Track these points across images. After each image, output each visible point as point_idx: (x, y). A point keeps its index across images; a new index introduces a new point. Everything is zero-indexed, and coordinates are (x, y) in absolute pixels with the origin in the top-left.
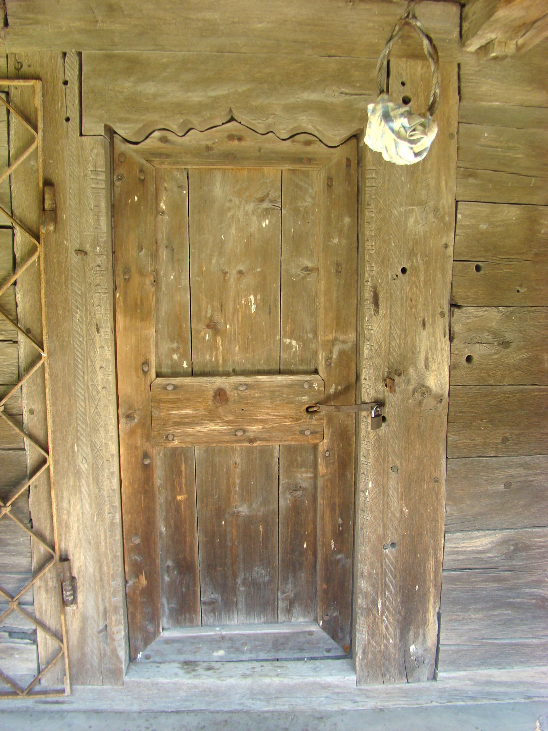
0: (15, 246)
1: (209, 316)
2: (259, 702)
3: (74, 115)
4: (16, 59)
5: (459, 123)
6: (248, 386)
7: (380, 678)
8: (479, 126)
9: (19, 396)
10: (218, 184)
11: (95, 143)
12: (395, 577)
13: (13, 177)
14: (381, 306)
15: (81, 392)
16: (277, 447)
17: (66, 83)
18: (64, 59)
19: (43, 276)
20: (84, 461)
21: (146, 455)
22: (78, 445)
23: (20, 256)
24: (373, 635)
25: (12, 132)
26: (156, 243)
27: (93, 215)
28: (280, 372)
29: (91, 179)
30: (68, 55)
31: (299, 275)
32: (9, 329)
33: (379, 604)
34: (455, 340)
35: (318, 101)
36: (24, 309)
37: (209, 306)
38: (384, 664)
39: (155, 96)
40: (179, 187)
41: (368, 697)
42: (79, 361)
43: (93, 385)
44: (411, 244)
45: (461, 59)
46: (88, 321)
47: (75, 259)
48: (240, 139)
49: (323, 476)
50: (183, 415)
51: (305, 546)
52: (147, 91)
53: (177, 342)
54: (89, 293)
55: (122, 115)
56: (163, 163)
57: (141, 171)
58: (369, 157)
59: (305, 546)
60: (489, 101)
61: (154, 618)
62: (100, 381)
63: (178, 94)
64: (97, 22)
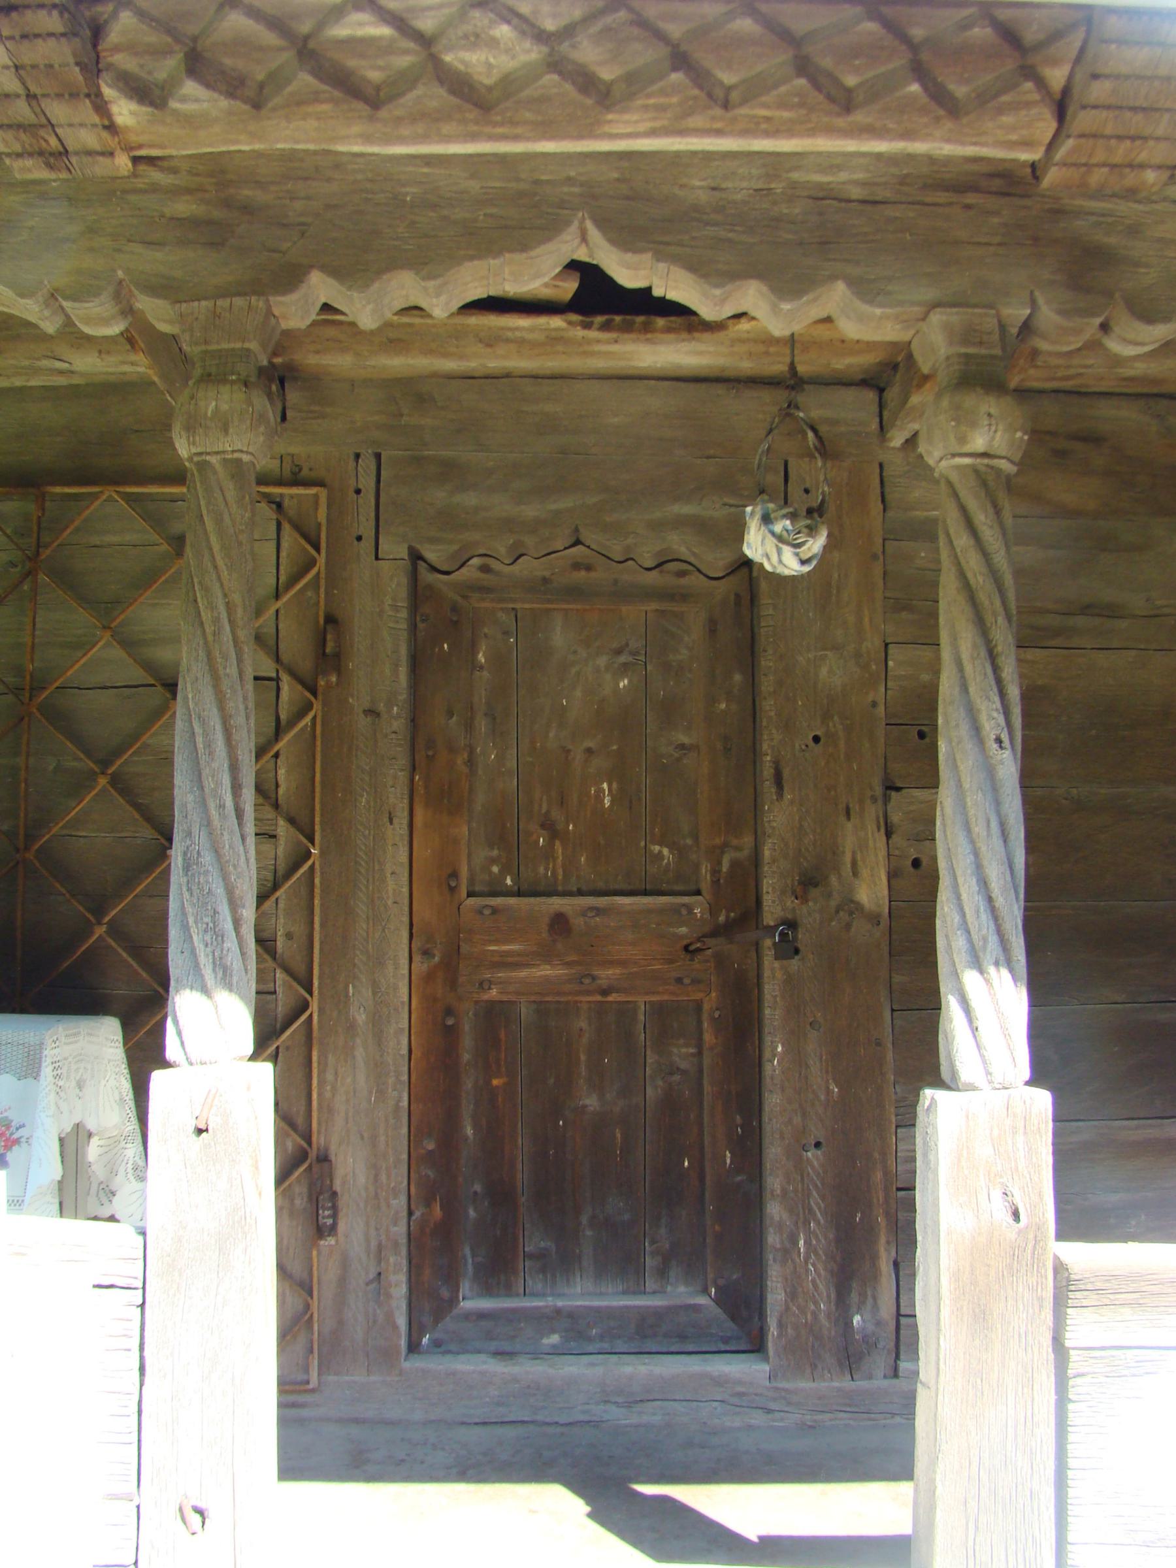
0: (280, 704)
1: (544, 810)
2: (613, 1408)
3: (368, 531)
4: (293, 462)
5: (884, 540)
6: (598, 911)
7: (808, 1371)
10: (558, 629)
12: (823, 1198)
14: (786, 789)
15: (362, 909)
16: (643, 1007)
17: (358, 492)
18: (357, 462)
19: (319, 743)
20: (362, 1009)
21: (449, 1012)
22: (354, 987)
24: (792, 1295)
25: (283, 554)
26: (472, 708)
28: (645, 893)
30: (362, 456)
31: (672, 755)
33: (801, 1243)
34: (894, 836)
37: (545, 797)
38: (813, 1346)
41: (789, 1404)
44: (825, 701)
47: (363, 722)
48: (589, 568)
49: (711, 1049)
50: (504, 952)
51: (686, 1164)
53: (499, 849)
58: (764, 586)
59: (686, 1164)
61: (451, 1277)
64: (402, 415)
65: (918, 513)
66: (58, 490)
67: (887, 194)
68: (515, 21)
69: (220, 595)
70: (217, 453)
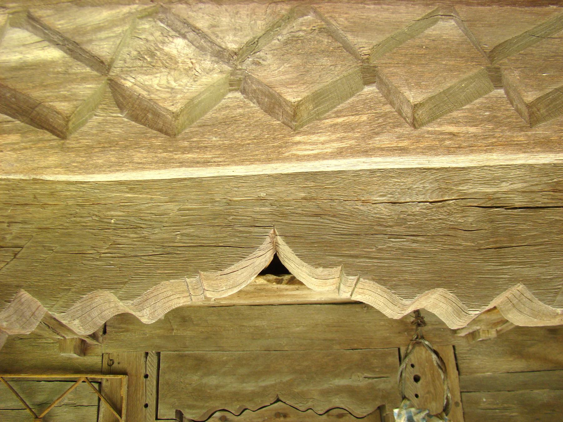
3: (152, 402)
4: (109, 357)
5: (461, 392)
8: (478, 394)
17: (146, 376)
18: (146, 358)
25: (101, 415)
30: (149, 355)
35: (347, 385)
39: (217, 387)
45: (455, 342)
52: (211, 383)
55: (190, 403)
60: (481, 373)
63: (235, 385)
64: (173, 330)
65: (479, 374)
67: (541, 201)
68: (191, 35)
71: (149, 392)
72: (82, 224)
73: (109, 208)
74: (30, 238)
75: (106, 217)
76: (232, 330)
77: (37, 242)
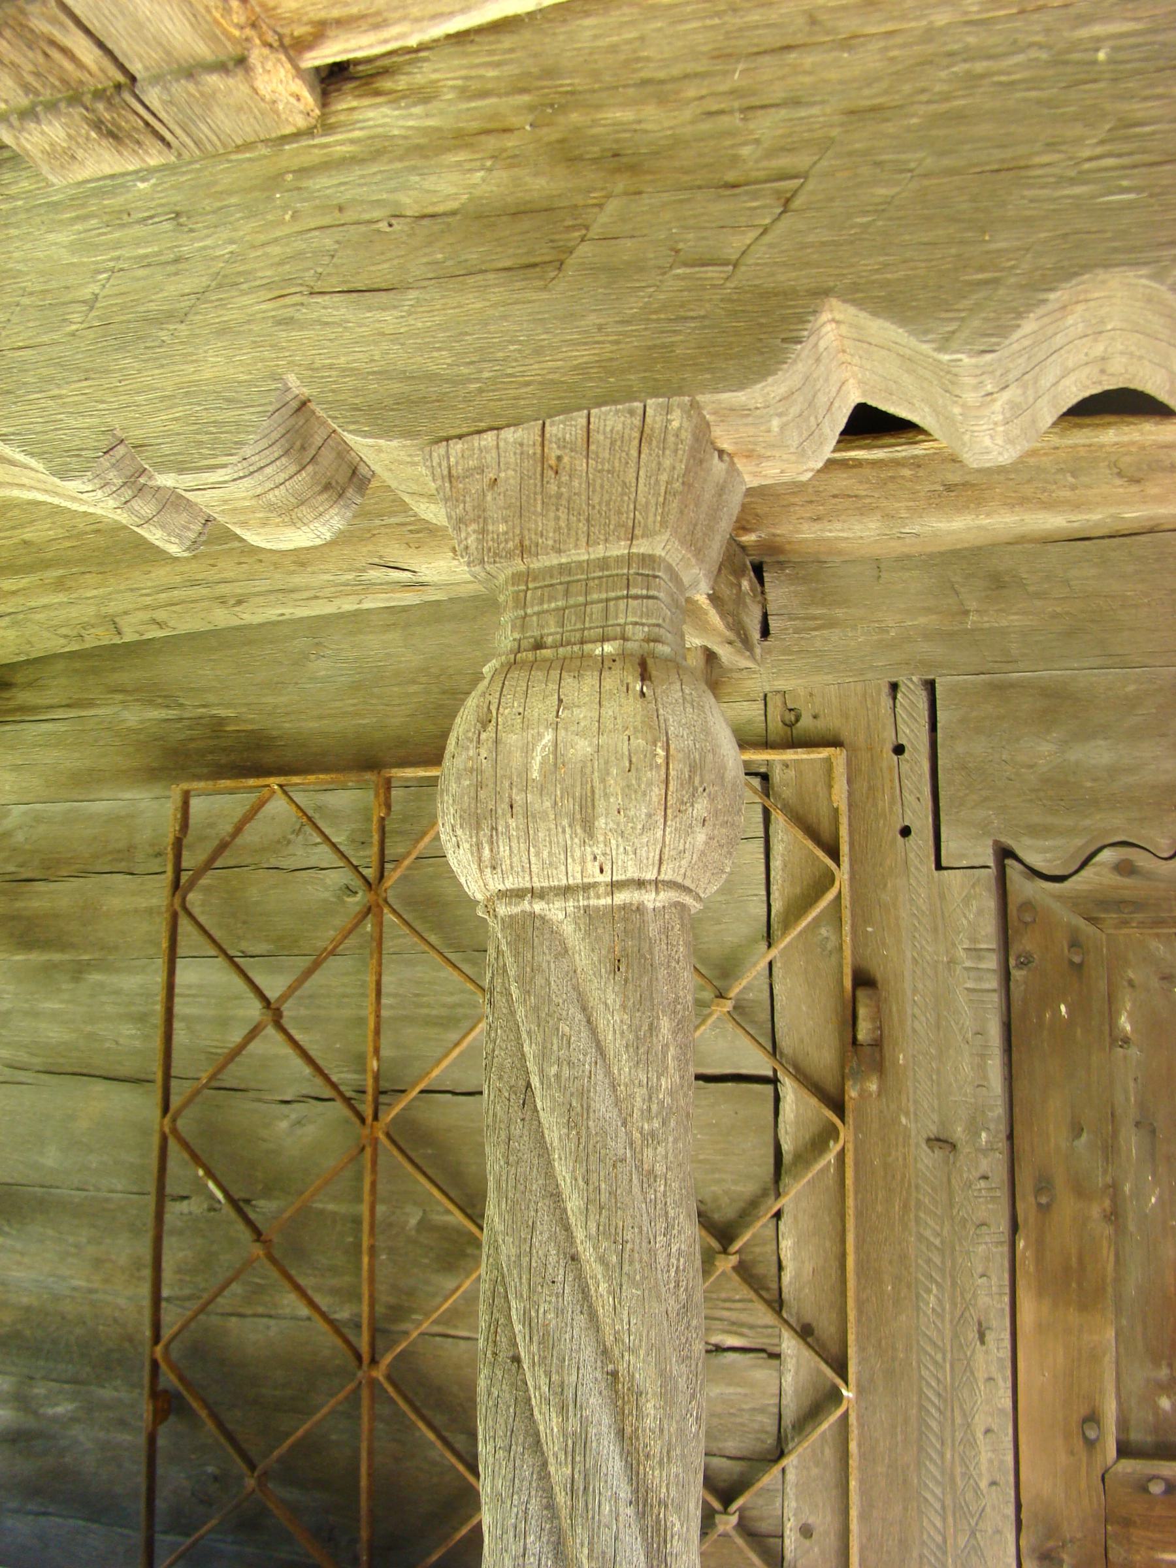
0: (781, 1125)
3: (922, 824)
9: (777, 1490)
11: (973, 886)
13: (779, 965)
17: (899, 750)
18: (894, 698)
19: (850, 1202)
23: (792, 1148)
25: (776, 864)
26: (1112, 1115)
27: (972, 1055)
29: (966, 969)
30: (902, 688)
32: (760, 1322)
36: (797, 1275)
39: (1113, 772)
40: (1163, 978)
42: (933, 1411)
43: (966, 1475)
46: (958, 1313)
47: (927, 1160)
52: (1093, 762)
54: (961, 1244)
55: (1036, 819)
56: (1125, 923)
57: (1075, 944)
62: (984, 1466)
64: (966, 613)
66: (410, 773)
69: (588, 1353)
70: (566, 891)
71: (911, 792)
72: (996, 79)
73: (1079, 16)
74: (825, 145)
75: (1074, 46)
76: (1149, 605)
77: (850, 154)
